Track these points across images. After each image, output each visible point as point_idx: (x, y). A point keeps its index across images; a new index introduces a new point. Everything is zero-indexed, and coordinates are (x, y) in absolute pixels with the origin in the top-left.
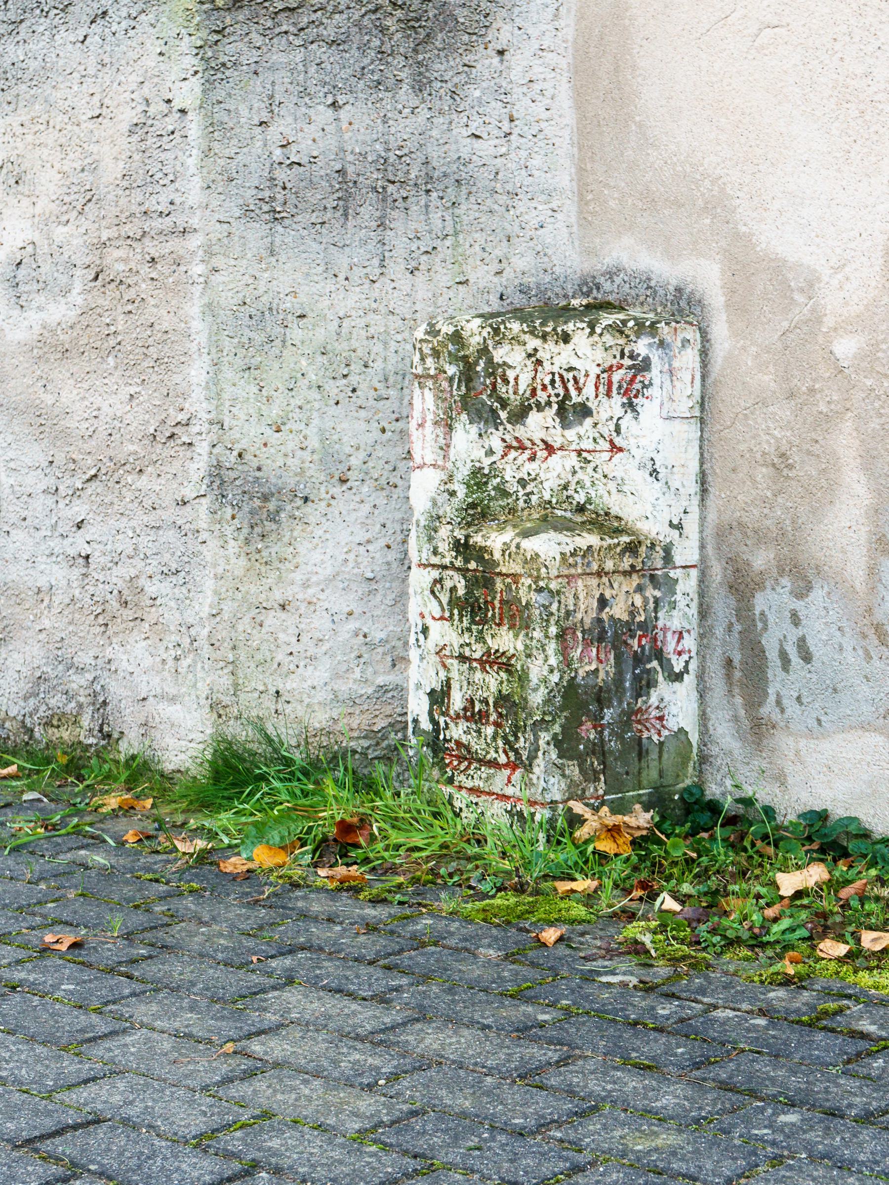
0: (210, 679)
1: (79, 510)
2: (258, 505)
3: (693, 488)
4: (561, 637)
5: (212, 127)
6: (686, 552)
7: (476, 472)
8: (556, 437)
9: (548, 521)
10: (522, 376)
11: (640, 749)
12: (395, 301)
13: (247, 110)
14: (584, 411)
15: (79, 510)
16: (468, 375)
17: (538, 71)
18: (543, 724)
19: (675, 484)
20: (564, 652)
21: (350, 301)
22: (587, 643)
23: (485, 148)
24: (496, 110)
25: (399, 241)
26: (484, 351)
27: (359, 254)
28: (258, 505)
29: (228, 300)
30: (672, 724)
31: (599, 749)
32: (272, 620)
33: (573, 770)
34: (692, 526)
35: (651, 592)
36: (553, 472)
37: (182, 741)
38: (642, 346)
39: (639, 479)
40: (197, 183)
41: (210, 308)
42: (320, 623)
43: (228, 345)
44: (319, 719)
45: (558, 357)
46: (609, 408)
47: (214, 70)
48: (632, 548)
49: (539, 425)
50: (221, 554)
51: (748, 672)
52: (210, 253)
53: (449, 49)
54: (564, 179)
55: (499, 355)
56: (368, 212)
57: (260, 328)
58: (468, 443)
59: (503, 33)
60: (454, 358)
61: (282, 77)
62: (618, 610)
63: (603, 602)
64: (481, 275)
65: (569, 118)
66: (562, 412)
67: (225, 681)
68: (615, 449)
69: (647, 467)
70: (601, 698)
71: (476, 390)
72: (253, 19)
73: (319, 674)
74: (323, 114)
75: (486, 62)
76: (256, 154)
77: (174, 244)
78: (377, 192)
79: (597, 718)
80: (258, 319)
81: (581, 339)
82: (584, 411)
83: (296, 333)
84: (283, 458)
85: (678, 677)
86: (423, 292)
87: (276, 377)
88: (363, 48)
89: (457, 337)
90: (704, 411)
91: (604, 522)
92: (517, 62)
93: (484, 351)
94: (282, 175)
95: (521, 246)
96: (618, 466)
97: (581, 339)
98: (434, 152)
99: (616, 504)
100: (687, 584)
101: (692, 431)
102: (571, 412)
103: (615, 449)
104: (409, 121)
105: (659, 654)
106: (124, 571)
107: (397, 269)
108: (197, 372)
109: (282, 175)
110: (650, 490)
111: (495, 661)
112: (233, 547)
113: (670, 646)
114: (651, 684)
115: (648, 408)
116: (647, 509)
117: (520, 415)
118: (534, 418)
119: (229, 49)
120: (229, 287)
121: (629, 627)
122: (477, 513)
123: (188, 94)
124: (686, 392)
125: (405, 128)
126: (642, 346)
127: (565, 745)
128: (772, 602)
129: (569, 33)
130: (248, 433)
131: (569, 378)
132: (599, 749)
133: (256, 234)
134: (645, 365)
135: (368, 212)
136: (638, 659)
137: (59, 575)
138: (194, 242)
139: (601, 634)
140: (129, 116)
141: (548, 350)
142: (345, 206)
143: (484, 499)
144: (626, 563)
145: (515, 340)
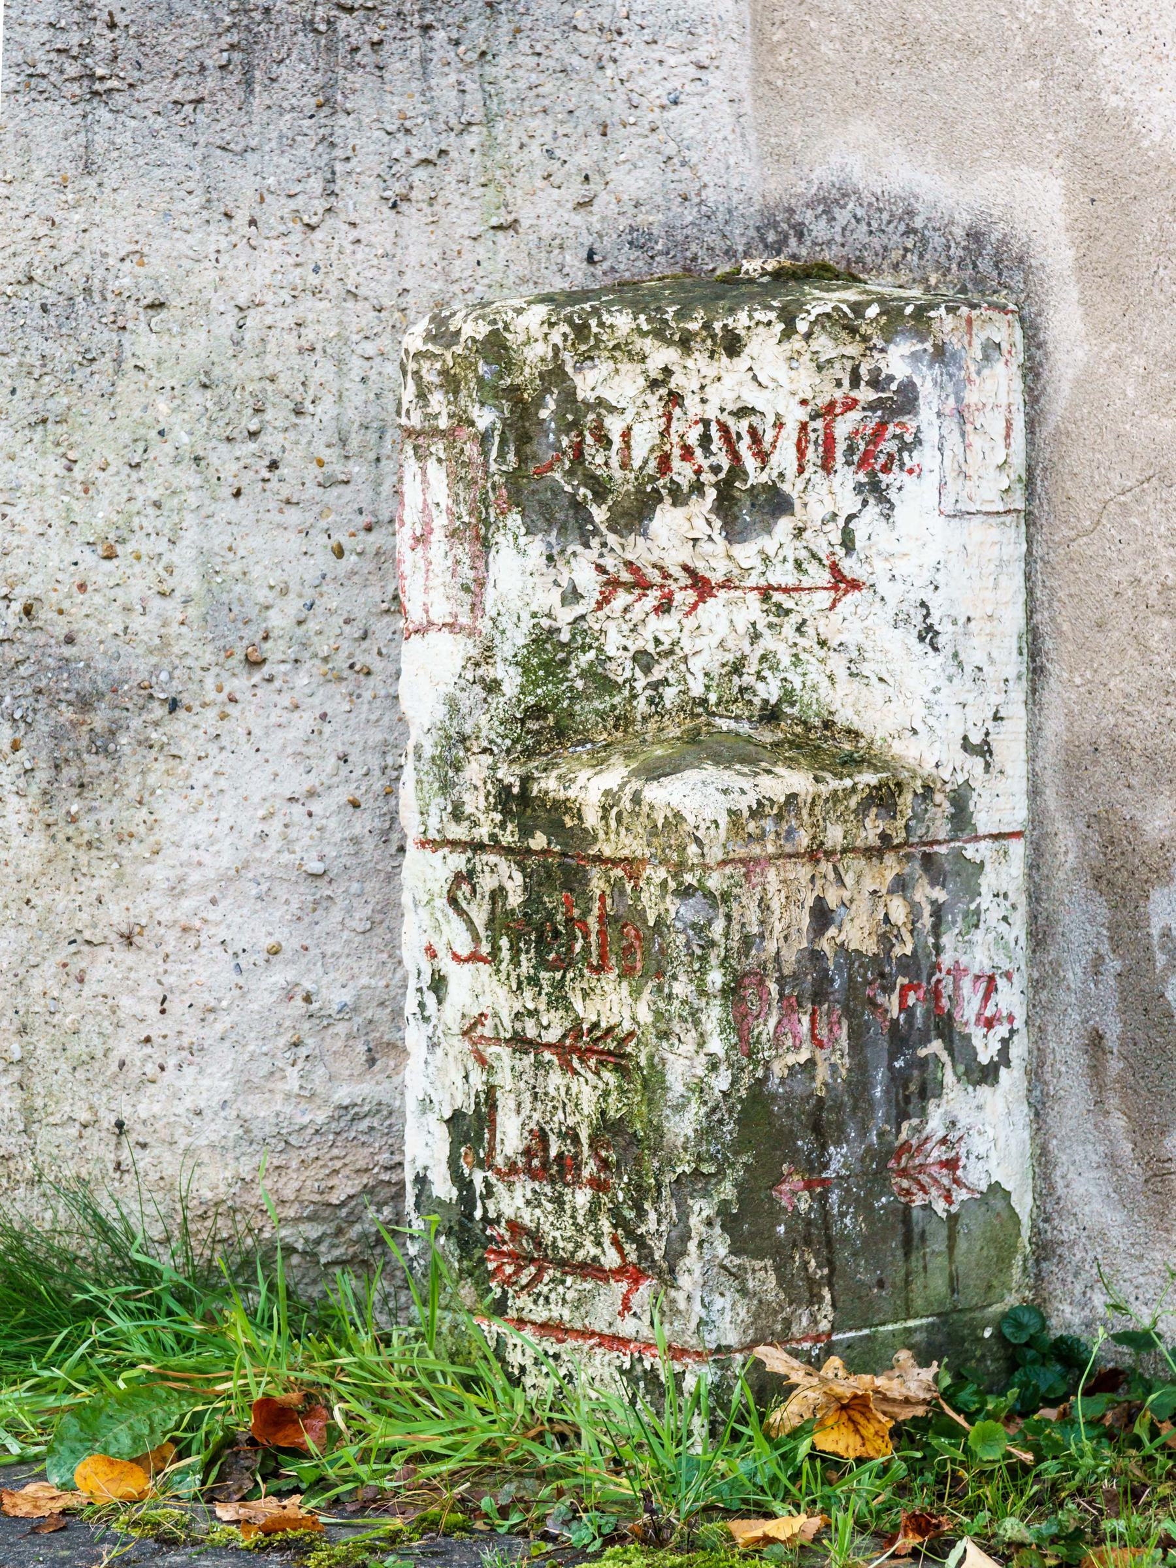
3: (1012, 664)
4: (732, 992)
6: (1001, 804)
7: (543, 639)
8: (716, 560)
12: (359, 268)
14: (775, 503)
16: (521, 428)
18: (696, 1182)
19: (973, 657)
20: (739, 1025)
21: (260, 271)
22: (790, 1006)
25: (365, 141)
26: (555, 375)
27: (279, 169)
30: (976, 1175)
31: (818, 1234)
32: (105, 968)
33: (765, 1280)
34: (1011, 747)
35: (926, 893)
36: (711, 634)
38: (898, 360)
39: (896, 647)
42: (210, 972)
44: (212, 1181)
46: (831, 494)
48: (883, 799)
49: (677, 533)
55: (588, 383)
56: (296, 76)
58: (524, 578)
60: (490, 393)
62: (856, 933)
63: (822, 916)
64: (545, 210)
66: (726, 504)
68: (842, 583)
70: (822, 1122)
71: (539, 460)
73: (209, 1083)
79: (814, 1166)
80: (60, 313)
81: (765, 347)
82: (775, 503)
83: (144, 344)
85: (987, 1075)
86: (419, 247)
87: (101, 438)
89: (496, 347)
90: (1035, 497)
91: (821, 743)
93: (555, 375)
97: (765, 347)
99: (847, 703)
100: (1004, 875)
101: (1008, 542)
102: (747, 505)
103: (842, 583)
105: (944, 1026)
107: (361, 198)
110: (919, 671)
113: (969, 1008)
114: (929, 1090)
115: (914, 494)
117: (635, 514)
121: (879, 969)
122: (545, 728)
124: (992, 459)
126: (898, 360)
131: (739, 431)
132: (818, 1234)
134: (905, 401)
135: (296, 76)
139: (818, 985)
141: (691, 370)
145: (623, 350)
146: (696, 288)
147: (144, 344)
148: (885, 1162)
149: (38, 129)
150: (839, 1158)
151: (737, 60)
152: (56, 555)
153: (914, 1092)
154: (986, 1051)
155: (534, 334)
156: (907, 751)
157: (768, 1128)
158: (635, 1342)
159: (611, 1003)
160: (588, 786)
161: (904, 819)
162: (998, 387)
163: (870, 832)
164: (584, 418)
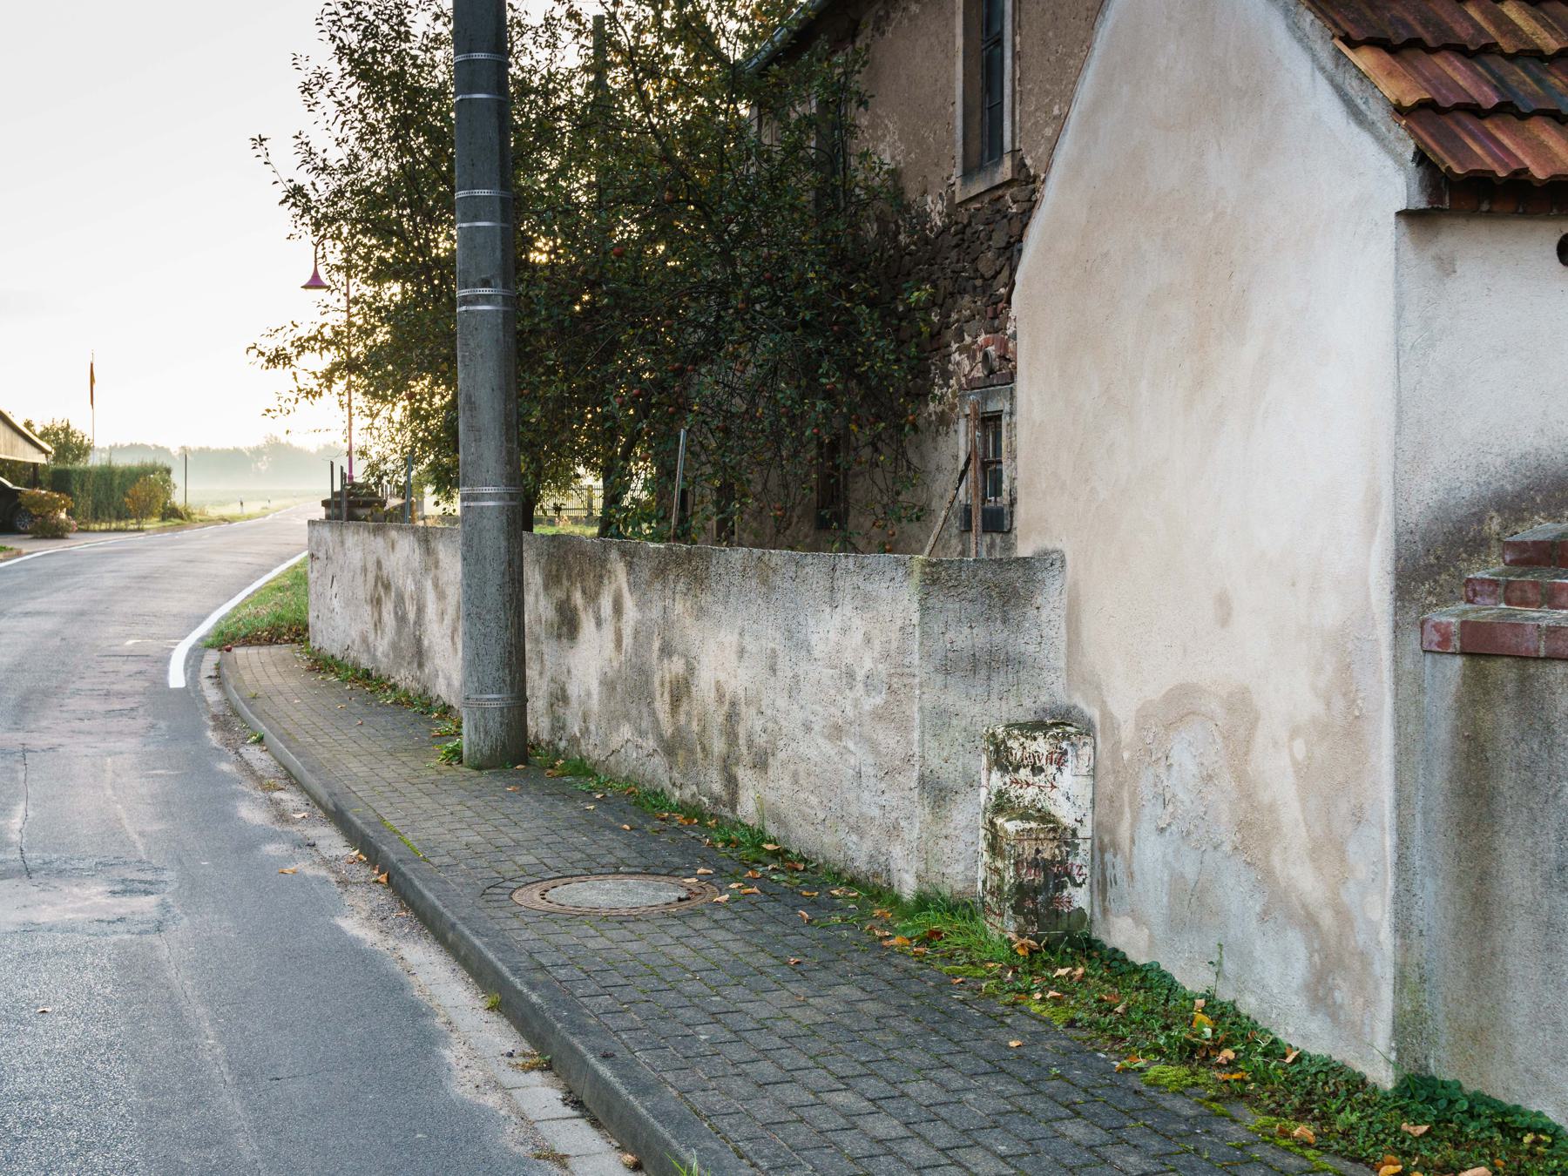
0: (918, 865)
1: (883, 786)
2: (937, 793)
3: (1089, 805)
4: (1016, 864)
5: (923, 633)
6: (1085, 832)
7: (999, 791)
8: (1031, 779)
9: (1025, 817)
10: (1018, 753)
11: (1058, 914)
12: (994, 711)
13: (937, 628)
14: (1041, 770)
15: (883, 786)
16: (997, 751)
17: (1053, 617)
18: (1007, 900)
19: (1079, 802)
20: (1017, 871)
21: (977, 709)
22: (1029, 868)
23: (1031, 648)
24: (1035, 632)
25: (995, 685)
26: (1003, 741)
27: (980, 690)
28: (937, 793)
29: (928, 706)
30: (1076, 905)
31: (1035, 912)
32: (942, 842)
33: (1021, 920)
34: (1088, 821)
35: (1064, 849)
36: (1029, 794)
37: (908, 886)
38: (1064, 745)
39: (1062, 800)
40: (917, 656)
41: (921, 709)
42: (961, 846)
43: (928, 724)
44: (959, 887)
45: (1032, 746)
46: (1051, 769)
47: (924, 609)
48: (1054, 830)
49: (1024, 773)
50: (923, 813)
51: (1102, 885)
52: (921, 685)
53: (1016, 606)
54: (1062, 664)
55: (1009, 743)
56: (983, 673)
57: (940, 719)
58: (997, 779)
59: (1039, 600)
60: (993, 744)
61: (951, 614)
62: (1047, 855)
63: (1038, 851)
64: (1028, 703)
65: (1065, 638)
66: (1033, 769)
67: (923, 866)
68: (1053, 787)
69: (1067, 794)
70: (1036, 891)
71: (1001, 759)
72: (941, 589)
73: (960, 868)
74: (966, 630)
75: (1032, 612)
76: (940, 646)
77: (910, 680)
78: (986, 665)
79: (1034, 900)
80: (940, 715)
81: (1041, 740)
82: (1041, 770)
83: (954, 722)
84: (949, 774)
85: (1080, 885)
86: (1005, 708)
87: (946, 740)
88: (983, 603)
89: (993, 735)
90: (1093, 773)
91: (1045, 817)
92: (1044, 613)
93: (1003, 741)
94: (950, 655)
95: (1044, 691)
96: (1055, 794)
97: (1041, 740)
98: (1010, 649)
99: (1053, 810)
100: (1085, 847)
101: (1089, 781)
102: (1037, 770)
103: (1053, 787)
104: (1000, 635)
105: (1069, 875)
106: (894, 815)
107: (994, 697)
108: (916, 735)
109: (950, 655)
110: (1066, 805)
111: (997, 871)
112: (927, 810)
113: (1075, 871)
114: (1064, 886)
115: (1067, 771)
116: (1066, 814)
117: (1016, 769)
118: (1022, 771)
119: (931, 602)
120: (929, 699)
121: (1052, 862)
122: (999, 809)
123: (916, 618)
124: (1084, 765)
125: (998, 638)
126: (1064, 745)
127: (1017, 909)
128: (1108, 856)
129: (1065, 601)
130: (935, 762)
131: (1036, 755)
132: (1035, 912)
133: (939, 678)
134: (1065, 753)
135: (983, 673)
136: (1057, 876)
137: (876, 812)
138: (917, 680)
139: (1035, 864)
140: (899, 623)
141: (1028, 743)
142: (974, 670)
143: (1002, 804)
144: (1051, 835)
145: (1016, 738)
146: (1034, 727)
147: (954, 722)
148: (1051, 901)
149: (1499, 460)
150: (1040, 898)
151: (1064, 675)
152: (936, 761)
153: (1061, 887)
154: (1079, 880)
155: (1000, 731)
156: (1063, 820)
157: (1021, 890)
158: (1003, 927)
159: (999, 864)
160: (999, 821)
161: (1065, 837)
162: (1088, 750)
163: (1051, 835)
164: (1008, 750)
